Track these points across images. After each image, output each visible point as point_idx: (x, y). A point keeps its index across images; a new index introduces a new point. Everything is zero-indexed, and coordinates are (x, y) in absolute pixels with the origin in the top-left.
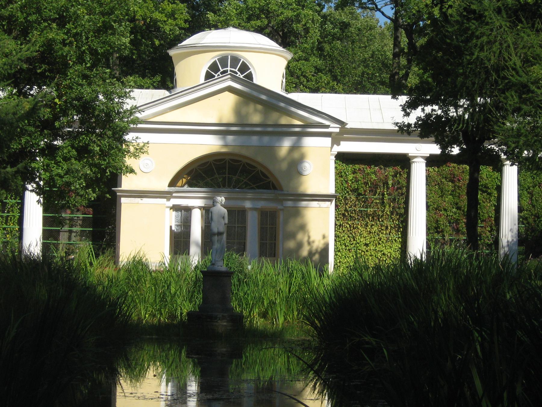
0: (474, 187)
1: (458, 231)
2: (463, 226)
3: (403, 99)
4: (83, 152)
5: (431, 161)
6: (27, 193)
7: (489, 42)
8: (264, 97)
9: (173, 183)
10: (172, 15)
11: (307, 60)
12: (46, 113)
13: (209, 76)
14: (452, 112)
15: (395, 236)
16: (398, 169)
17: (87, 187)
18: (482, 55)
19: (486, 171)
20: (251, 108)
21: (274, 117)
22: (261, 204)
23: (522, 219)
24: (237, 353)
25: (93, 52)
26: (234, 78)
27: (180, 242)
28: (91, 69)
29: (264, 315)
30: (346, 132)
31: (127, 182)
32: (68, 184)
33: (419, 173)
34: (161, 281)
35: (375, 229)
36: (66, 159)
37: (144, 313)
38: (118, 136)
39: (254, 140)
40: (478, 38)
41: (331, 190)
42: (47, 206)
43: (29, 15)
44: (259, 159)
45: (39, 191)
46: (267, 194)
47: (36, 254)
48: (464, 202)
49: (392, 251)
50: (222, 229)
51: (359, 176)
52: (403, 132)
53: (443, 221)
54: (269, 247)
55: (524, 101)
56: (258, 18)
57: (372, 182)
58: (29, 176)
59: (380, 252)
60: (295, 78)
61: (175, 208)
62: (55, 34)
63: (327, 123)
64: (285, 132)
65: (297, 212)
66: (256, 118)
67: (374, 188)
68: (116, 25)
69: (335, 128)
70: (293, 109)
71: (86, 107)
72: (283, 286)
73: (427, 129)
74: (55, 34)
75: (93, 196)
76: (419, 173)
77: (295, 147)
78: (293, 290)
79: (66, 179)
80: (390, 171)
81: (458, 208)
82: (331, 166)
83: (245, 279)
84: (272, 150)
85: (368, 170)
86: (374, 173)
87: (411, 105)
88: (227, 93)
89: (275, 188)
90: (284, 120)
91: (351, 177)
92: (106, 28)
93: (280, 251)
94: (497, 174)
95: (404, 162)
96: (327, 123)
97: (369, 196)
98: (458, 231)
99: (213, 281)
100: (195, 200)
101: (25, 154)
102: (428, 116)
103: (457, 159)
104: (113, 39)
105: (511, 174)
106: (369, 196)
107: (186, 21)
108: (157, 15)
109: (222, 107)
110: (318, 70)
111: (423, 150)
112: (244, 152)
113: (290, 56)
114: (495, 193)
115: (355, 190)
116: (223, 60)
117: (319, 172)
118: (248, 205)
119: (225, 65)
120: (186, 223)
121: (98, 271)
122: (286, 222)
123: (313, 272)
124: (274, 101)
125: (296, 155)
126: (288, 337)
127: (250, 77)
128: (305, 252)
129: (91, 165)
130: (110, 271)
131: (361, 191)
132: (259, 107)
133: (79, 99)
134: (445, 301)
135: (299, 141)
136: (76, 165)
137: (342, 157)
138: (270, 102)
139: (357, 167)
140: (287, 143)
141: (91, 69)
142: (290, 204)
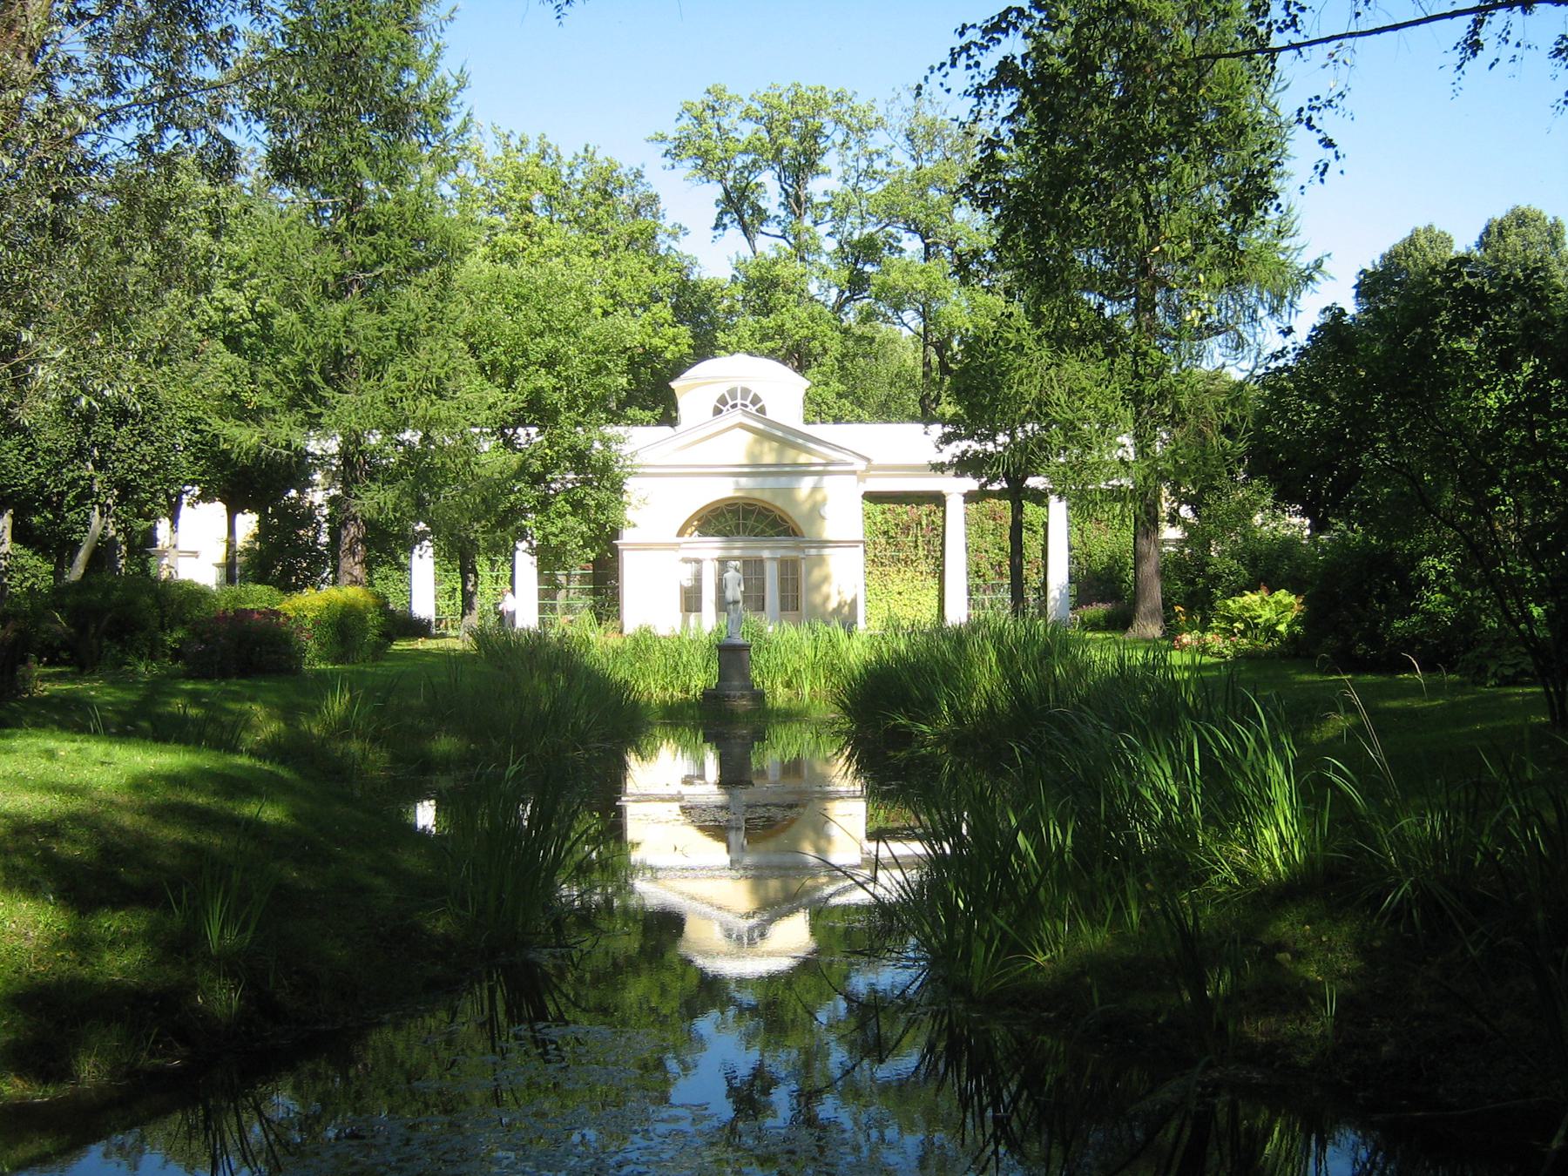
0: (1017, 528)
1: (1001, 575)
2: (1006, 569)
3: (937, 430)
4: (578, 506)
5: (970, 497)
6: (518, 554)
7: (1029, 375)
8: (780, 434)
9: (681, 533)
10: (674, 340)
11: (827, 384)
12: (536, 466)
13: (717, 411)
14: (990, 447)
15: (932, 583)
16: (933, 507)
17: (584, 546)
18: (1021, 389)
19: (1029, 507)
20: (766, 446)
21: (791, 455)
22: (779, 554)
23: (1073, 559)
24: (760, 736)
25: (587, 395)
26: (746, 414)
27: (691, 600)
28: (584, 415)
29: (788, 685)
30: (872, 468)
31: (627, 536)
32: (564, 543)
33: (956, 510)
34: (675, 657)
35: (909, 575)
36: (561, 515)
37: (654, 689)
38: (617, 488)
39: (770, 482)
40: (1016, 370)
41: (861, 538)
42: (543, 566)
43: (514, 358)
44: (778, 504)
45: (534, 551)
46: (788, 541)
47: (825, 589)
48: (1007, 544)
49: (927, 616)
50: (739, 597)
51: (889, 516)
52: (939, 468)
53: (985, 565)
54: (792, 601)
55: (1069, 439)
56: (772, 339)
57: (904, 518)
58: (521, 534)
59: (917, 608)
60: (816, 409)
61: (686, 561)
62: (544, 381)
63: (849, 459)
64: (799, 471)
65: (820, 560)
66: (769, 458)
67: (906, 529)
68: (611, 365)
69: (860, 465)
70: (812, 445)
71: (580, 459)
72: (809, 652)
73: (965, 465)
74: (544, 381)
75: (592, 556)
76: (956, 510)
77: (815, 489)
78: (819, 655)
79: (562, 538)
80: (925, 509)
81: (1001, 549)
82: (857, 506)
83: (767, 645)
84: (789, 492)
85: (899, 510)
86: (905, 512)
87: (947, 439)
88: (738, 430)
89: (796, 535)
90: (803, 458)
91: (879, 518)
92: (600, 369)
93: (803, 605)
94: (1042, 510)
95: (938, 499)
96: (849, 459)
97: (901, 538)
98: (1001, 575)
99: (731, 656)
100: (710, 549)
101: (516, 512)
102: (964, 453)
103: (1000, 495)
104: (608, 381)
105: (1058, 511)
106: (901, 538)
107: (690, 346)
108: (656, 341)
109: (736, 447)
110: (840, 395)
111: (956, 487)
112: (757, 495)
113: (807, 384)
114: (1042, 531)
115: (886, 533)
116: (733, 393)
117: (841, 513)
118: (766, 554)
119: (734, 397)
120: (698, 578)
121: (600, 642)
122: (809, 572)
123: (841, 632)
124: (791, 438)
125: (819, 497)
126: (814, 714)
127: (762, 410)
128: (832, 605)
129: (588, 521)
130: (614, 641)
131: (892, 533)
132: (775, 445)
133: (572, 448)
134: (986, 676)
135: (820, 481)
136: (571, 521)
137: (872, 497)
138: (785, 439)
139: (886, 506)
140: (805, 485)
141: (584, 415)
142: (813, 552)
